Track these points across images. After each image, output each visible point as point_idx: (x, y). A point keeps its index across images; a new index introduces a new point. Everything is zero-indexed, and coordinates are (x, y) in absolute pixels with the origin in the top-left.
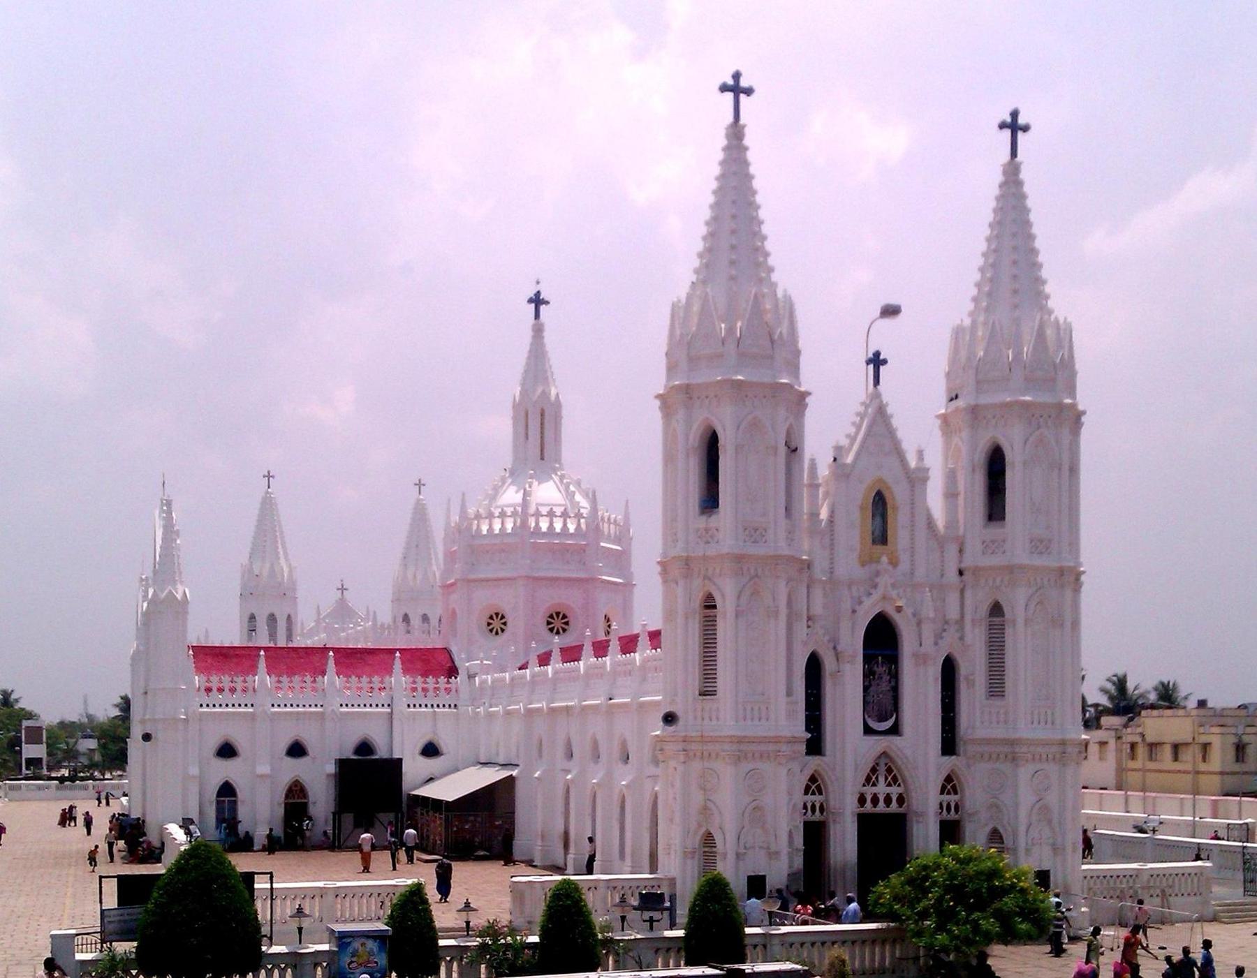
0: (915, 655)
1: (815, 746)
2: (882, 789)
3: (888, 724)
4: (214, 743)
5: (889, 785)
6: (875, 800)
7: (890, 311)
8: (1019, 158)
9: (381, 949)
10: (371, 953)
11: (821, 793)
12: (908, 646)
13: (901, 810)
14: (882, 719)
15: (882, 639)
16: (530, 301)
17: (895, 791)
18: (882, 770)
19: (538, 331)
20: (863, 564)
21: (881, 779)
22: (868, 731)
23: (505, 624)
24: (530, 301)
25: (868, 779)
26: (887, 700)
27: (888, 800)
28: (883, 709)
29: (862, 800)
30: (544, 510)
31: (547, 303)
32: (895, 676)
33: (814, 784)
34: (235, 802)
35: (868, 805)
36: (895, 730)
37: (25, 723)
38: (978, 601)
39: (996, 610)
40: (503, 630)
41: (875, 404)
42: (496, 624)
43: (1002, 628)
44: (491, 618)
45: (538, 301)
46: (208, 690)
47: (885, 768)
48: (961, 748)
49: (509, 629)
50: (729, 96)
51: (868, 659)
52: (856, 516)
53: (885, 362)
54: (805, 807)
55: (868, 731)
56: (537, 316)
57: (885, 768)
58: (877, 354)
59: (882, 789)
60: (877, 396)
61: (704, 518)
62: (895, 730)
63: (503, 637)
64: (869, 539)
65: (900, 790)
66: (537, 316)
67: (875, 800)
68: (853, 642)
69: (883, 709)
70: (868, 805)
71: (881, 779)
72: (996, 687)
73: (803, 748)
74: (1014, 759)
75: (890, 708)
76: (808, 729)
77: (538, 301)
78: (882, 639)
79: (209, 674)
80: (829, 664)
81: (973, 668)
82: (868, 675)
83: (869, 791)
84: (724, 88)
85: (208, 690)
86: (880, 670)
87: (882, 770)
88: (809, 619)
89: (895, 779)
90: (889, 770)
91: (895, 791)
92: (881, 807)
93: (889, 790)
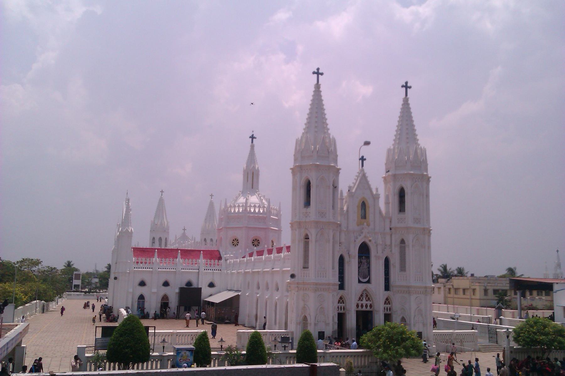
1: (342, 287)
2: (364, 302)
6: (362, 306)
7: (367, 143)
8: (408, 96)
9: (191, 354)
10: (188, 356)
12: (373, 253)
13: (371, 310)
14: (365, 278)
15: (364, 251)
16: (250, 137)
17: (369, 303)
18: (364, 295)
20: (358, 225)
21: (364, 299)
22: (360, 282)
24: (250, 137)
25: (360, 298)
27: (366, 306)
28: (365, 275)
29: (358, 306)
30: (252, 205)
33: (341, 300)
34: (144, 302)
35: (360, 307)
36: (369, 282)
37: (75, 273)
38: (396, 239)
39: (403, 242)
42: (235, 242)
43: (404, 248)
45: (252, 137)
46: (137, 263)
47: (365, 295)
48: (391, 288)
49: (239, 244)
50: (316, 75)
54: (338, 308)
55: (360, 282)
56: (252, 142)
57: (365, 295)
58: (363, 157)
59: (364, 302)
62: (369, 282)
64: (360, 217)
65: (371, 303)
66: (252, 142)
67: (362, 306)
68: (355, 252)
69: (365, 275)
70: (360, 307)
71: (364, 299)
72: (403, 268)
73: (338, 287)
74: (409, 293)
75: (367, 274)
76: (339, 281)
77: (252, 137)
78: (364, 251)
80: (346, 259)
81: (395, 262)
82: (360, 263)
85: (137, 263)
86: (364, 261)
87: (364, 295)
88: (340, 243)
89: (369, 299)
90: (367, 296)
91: (369, 303)
92: (364, 309)
93: (367, 302)
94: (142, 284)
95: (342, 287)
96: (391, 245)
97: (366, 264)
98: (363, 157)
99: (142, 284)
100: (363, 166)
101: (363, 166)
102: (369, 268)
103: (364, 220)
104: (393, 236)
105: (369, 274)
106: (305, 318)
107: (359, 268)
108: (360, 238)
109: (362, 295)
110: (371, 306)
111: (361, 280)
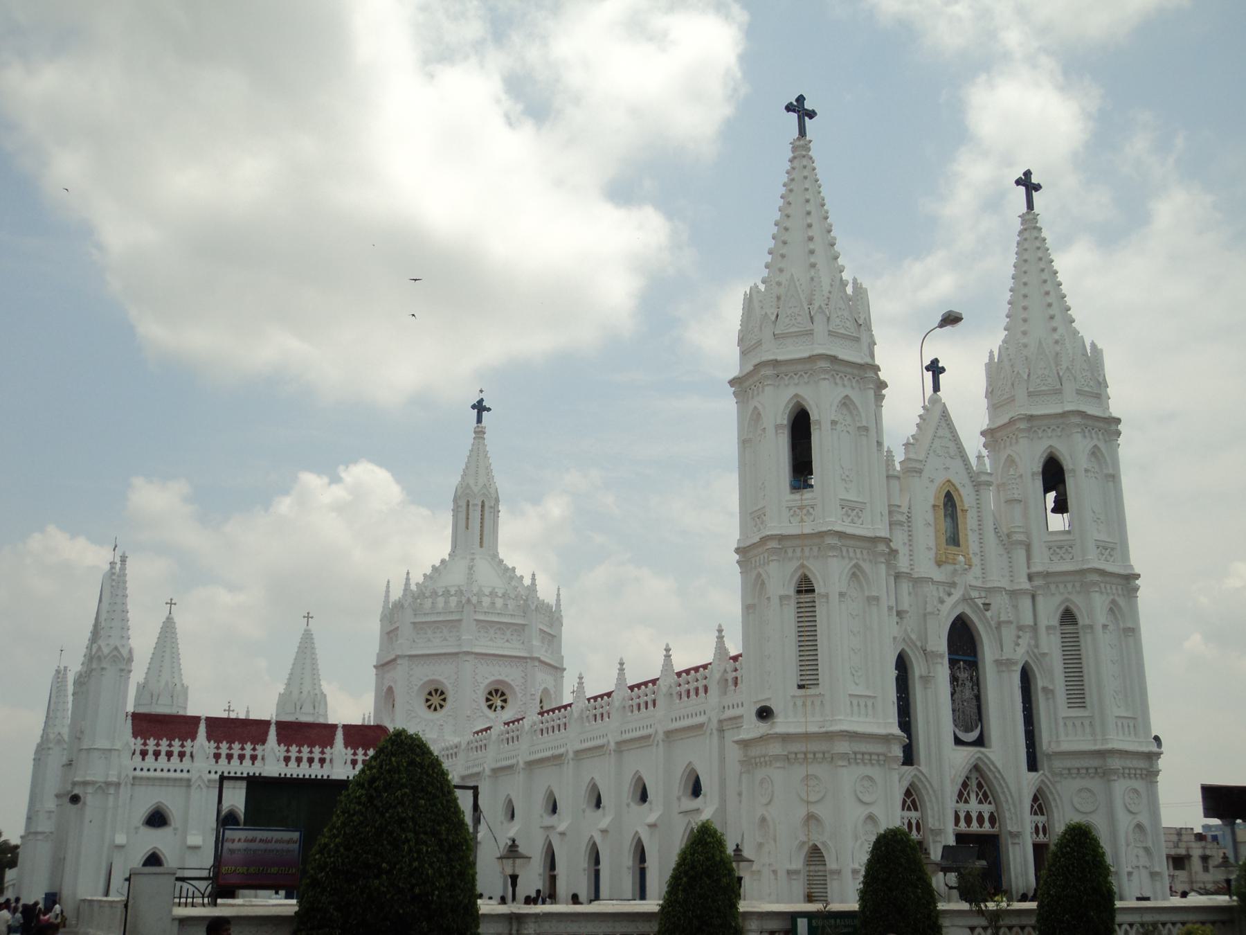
0: (998, 663)
1: (909, 758)
2: (974, 806)
3: (973, 736)
4: (143, 811)
5: (980, 802)
7: (951, 319)
8: (1036, 210)
11: (916, 809)
12: (989, 653)
13: (995, 830)
14: (968, 730)
15: (963, 640)
16: (474, 407)
17: (986, 809)
18: (973, 785)
19: (480, 433)
20: (939, 564)
21: (973, 796)
22: (958, 742)
23: (444, 700)
24: (474, 407)
25: (960, 795)
26: (971, 709)
28: (971, 719)
30: (487, 591)
31: (489, 410)
32: (977, 683)
35: (962, 824)
38: (1049, 613)
39: (1068, 617)
40: (435, 709)
41: (937, 413)
42: (435, 700)
43: (1076, 636)
44: (430, 694)
45: (480, 407)
46: (144, 754)
47: (978, 782)
49: (448, 705)
50: (794, 117)
51: (953, 663)
52: (930, 517)
53: (943, 370)
56: (479, 420)
57: (978, 782)
58: (935, 362)
59: (974, 806)
60: (935, 401)
61: (797, 496)
62: (980, 742)
63: (441, 714)
64: (943, 539)
66: (479, 420)
68: (939, 643)
69: (971, 719)
70: (975, 824)
71: (973, 796)
72: (1077, 697)
74: (1106, 774)
75: (975, 717)
77: (480, 407)
78: (963, 640)
79: (288, 745)
81: (1051, 678)
82: (954, 679)
83: (963, 808)
84: (789, 108)
85: (144, 754)
86: (963, 675)
87: (973, 785)
89: (985, 796)
90: (980, 786)
91: (986, 809)
92: (975, 827)
94: (157, 819)
95: (909, 758)
96: (1035, 628)
97: (969, 684)
98: (935, 362)
99: (157, 819)
100: (936, 388)
101: (936, 388)
102: (978, 698)
103: (953, 549)
104: (1040, 600)
105: (980, 719)
106: (815, 854)
107: (952, 695)
108: (950, 601)
109: (965, 785)
110: (993, 820)
111: (963, 736)
